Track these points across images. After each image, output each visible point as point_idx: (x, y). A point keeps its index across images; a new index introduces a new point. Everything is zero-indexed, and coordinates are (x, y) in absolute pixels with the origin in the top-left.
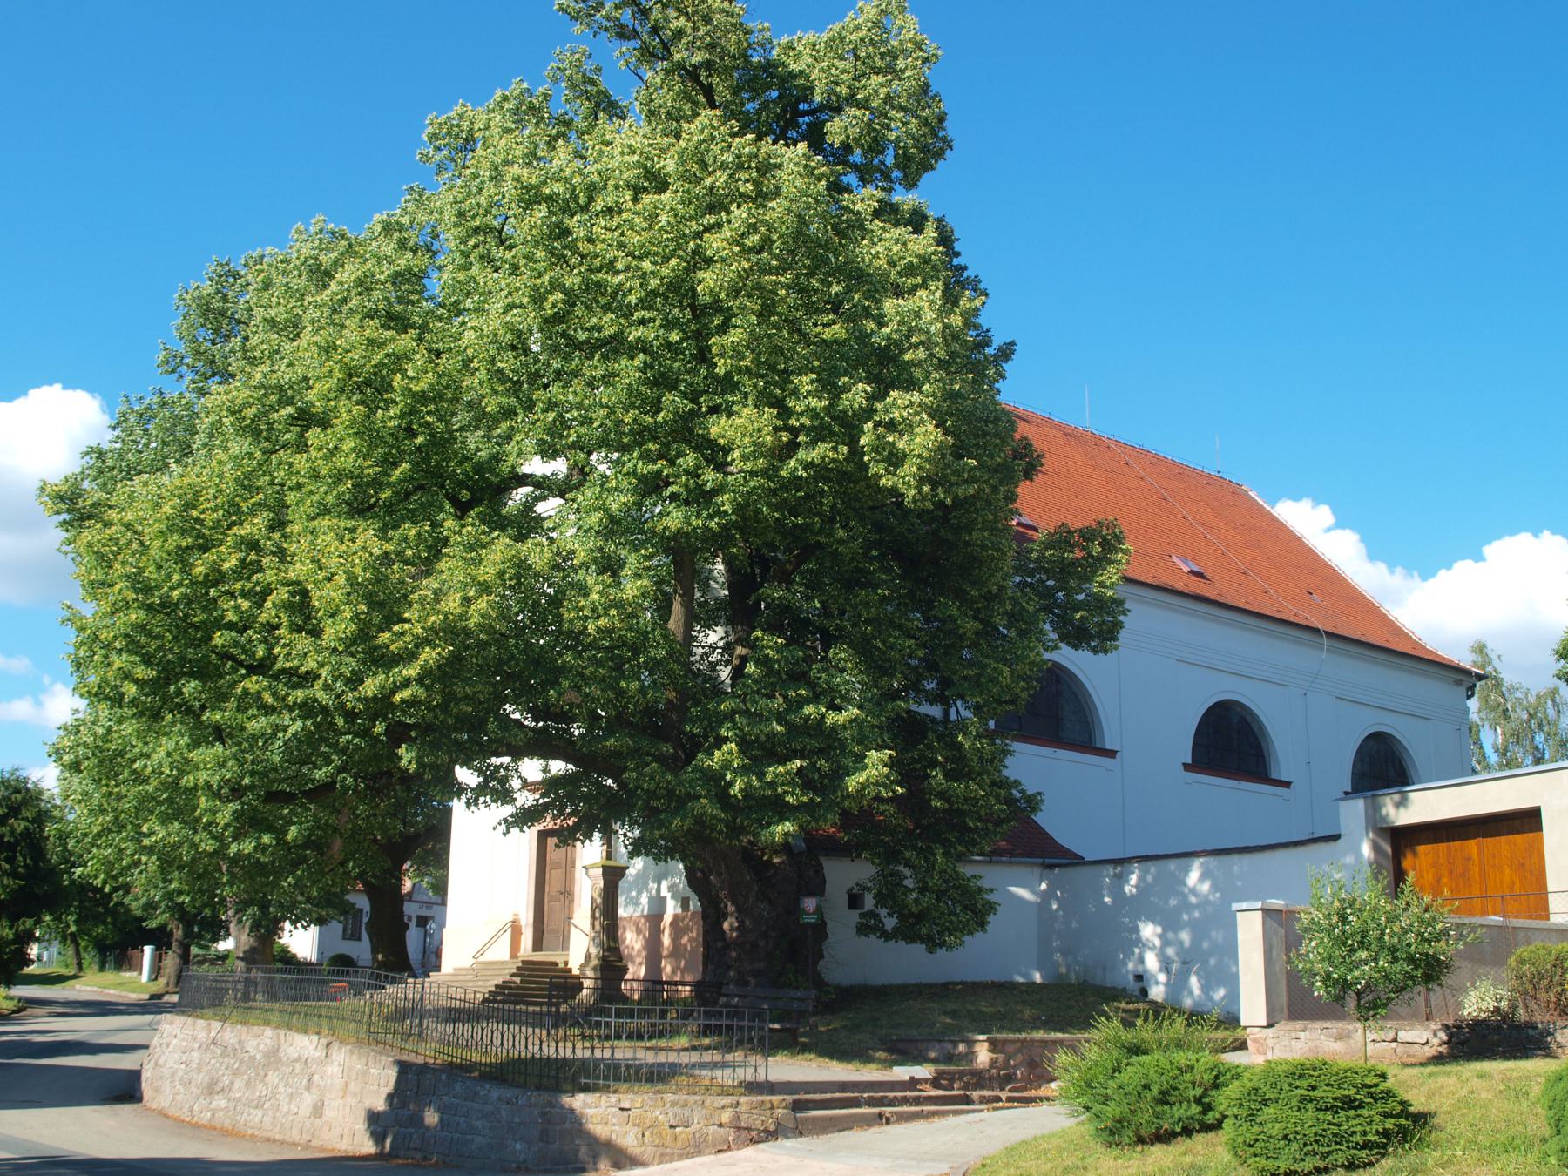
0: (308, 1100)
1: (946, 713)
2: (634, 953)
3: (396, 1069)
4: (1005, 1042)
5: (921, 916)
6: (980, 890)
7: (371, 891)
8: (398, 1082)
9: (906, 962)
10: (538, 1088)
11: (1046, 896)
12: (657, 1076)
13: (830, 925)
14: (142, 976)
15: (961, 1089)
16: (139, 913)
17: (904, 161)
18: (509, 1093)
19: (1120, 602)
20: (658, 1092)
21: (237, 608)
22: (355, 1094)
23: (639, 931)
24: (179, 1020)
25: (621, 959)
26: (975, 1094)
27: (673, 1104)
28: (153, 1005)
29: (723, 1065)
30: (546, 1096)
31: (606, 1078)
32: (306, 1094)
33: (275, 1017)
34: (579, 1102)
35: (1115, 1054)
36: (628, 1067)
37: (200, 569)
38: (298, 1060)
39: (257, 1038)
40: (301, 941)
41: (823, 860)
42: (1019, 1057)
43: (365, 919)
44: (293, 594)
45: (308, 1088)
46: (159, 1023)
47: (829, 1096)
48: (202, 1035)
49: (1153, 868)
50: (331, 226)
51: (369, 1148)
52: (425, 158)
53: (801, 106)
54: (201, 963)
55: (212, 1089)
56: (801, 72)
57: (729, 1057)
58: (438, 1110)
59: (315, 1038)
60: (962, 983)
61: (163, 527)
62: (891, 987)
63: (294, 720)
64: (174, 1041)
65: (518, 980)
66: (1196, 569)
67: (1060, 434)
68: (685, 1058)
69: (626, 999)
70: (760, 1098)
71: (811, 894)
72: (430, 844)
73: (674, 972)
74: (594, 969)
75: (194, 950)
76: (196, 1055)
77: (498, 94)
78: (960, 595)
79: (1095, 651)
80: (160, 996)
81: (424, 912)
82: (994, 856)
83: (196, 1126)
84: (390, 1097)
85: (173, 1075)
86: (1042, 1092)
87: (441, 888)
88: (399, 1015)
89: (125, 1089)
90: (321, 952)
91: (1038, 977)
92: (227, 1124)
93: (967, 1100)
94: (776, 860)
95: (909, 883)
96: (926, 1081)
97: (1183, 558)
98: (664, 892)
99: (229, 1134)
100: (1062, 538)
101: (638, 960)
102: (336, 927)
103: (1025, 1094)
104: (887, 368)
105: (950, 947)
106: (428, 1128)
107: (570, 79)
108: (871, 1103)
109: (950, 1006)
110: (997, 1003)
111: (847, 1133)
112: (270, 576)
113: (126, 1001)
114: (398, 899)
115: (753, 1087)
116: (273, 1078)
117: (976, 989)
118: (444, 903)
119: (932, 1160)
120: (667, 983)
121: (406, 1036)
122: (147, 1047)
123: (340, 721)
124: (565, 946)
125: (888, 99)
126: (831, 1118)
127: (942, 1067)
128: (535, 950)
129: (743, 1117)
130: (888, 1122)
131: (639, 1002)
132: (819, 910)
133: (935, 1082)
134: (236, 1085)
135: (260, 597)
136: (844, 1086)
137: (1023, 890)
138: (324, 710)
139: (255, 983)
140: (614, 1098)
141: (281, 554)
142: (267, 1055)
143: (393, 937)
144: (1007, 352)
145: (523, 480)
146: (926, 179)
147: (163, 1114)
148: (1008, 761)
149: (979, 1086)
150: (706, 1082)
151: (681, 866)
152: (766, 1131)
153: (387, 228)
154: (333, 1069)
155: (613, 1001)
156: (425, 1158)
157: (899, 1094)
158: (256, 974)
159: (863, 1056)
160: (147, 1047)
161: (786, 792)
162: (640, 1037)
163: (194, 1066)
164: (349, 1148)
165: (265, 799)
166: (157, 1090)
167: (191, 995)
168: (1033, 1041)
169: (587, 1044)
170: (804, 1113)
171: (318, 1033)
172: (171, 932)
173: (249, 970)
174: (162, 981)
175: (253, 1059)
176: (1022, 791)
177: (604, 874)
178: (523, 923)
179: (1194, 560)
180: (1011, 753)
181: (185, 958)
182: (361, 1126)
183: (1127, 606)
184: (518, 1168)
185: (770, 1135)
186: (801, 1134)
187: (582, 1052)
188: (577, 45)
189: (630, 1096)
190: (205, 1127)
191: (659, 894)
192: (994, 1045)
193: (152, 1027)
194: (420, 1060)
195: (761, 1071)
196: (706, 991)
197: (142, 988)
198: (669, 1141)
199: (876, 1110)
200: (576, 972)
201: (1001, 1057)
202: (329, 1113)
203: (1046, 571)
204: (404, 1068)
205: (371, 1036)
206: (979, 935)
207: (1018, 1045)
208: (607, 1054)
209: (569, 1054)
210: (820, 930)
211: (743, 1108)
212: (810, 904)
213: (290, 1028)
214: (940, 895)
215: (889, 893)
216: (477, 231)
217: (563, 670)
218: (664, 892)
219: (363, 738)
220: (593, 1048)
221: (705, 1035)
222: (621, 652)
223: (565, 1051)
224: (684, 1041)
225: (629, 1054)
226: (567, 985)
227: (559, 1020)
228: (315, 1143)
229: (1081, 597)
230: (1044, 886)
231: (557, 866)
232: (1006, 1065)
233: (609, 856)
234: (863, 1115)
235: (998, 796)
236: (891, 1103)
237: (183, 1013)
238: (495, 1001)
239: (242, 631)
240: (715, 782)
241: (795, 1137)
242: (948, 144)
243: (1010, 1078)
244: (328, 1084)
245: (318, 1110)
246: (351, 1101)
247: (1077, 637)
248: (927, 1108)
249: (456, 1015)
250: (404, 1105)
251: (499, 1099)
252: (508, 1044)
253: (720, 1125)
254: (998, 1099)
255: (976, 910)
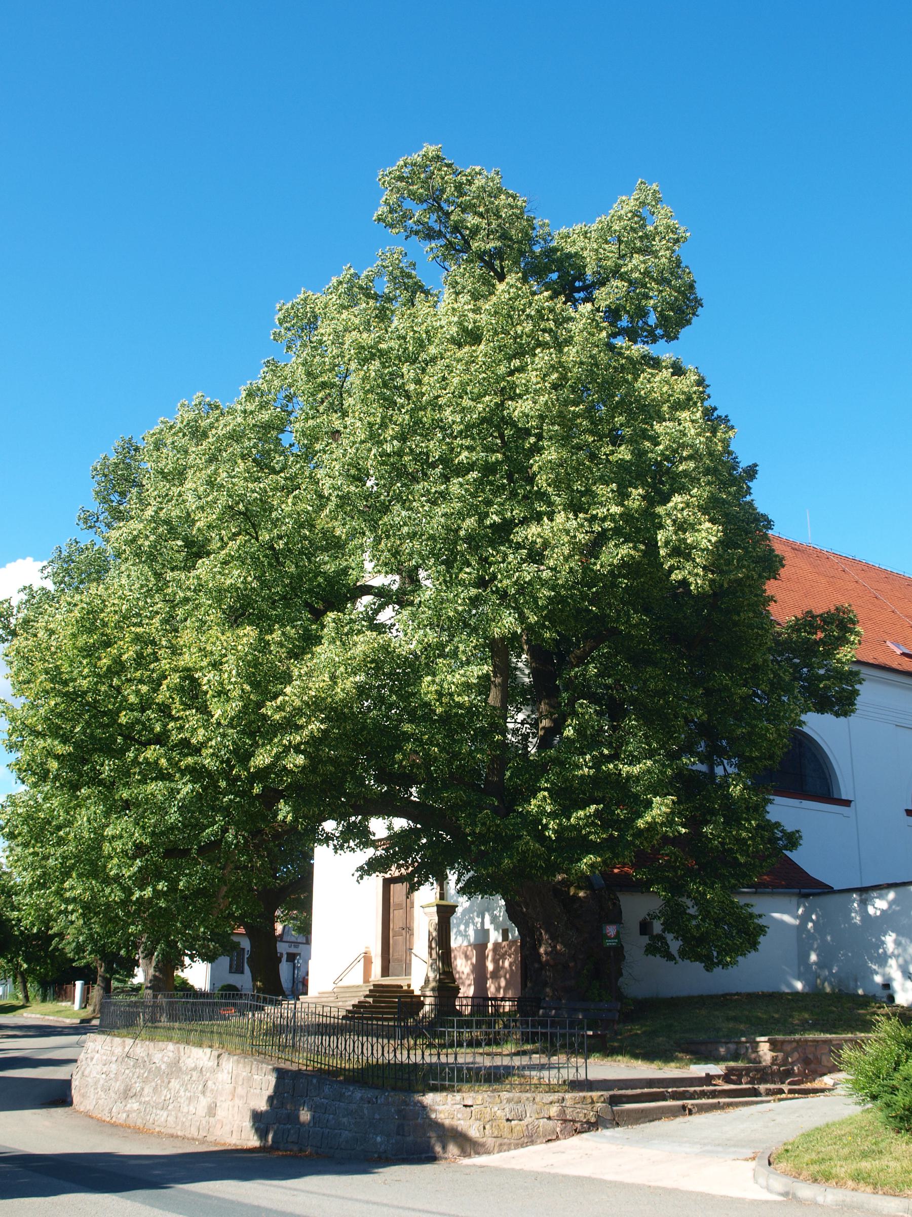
0: (204, 1102)
1: (712, 769)
2: (464, 977)
3: (275, 1075)
4: (783, 1042)
5: (702, 940)
6: (751, 916)
7: (252, 933)
8: (277, 1086)
9: (689, 978)
10: (394, 1089)
11: (805, 918)
12: (494, 1077)
13: (626, 948)
14: (72, 1008)
15: (750, 1084)
16: (71, 955)
17: (663, 319)
18: (370, 1094)
19: (857, 674)
20: (494, 1091)
21: (137, 692)
22: (241, 1097)
23: (467, 957)
24: (100, 1038)
25: (454, 981)
26: (762, 1087)
27: (509, 1101)
28: (82, 1028)
29: (549, 1067)
30: (402, 1096)
31: (451, 1079)
32: (201, 1097)
33: (176, 1034)
34: (429, 1099)
35: (895, 1048)
36: (469, 1069)
37: (105, 662)
38: (195, 1069)
39: (162, 1052)
40: (197, 974)
41: (618, 894)
42: (796, 1055)
43: (246, 956)
44: (183, 679)
45: (203, 1093)
46: (84, 1042)
47: (639, 1091)
48: (118, 1051)
49: (901, 889)
50: (208, 399)
51: (253, 1142)
52: (277, 336)
53: (577, 284)
54: (118, 994)
55: (127, 1094)
56: (576, 253)
57: (554, 1059)
58: (310, 1110)
59: (208, 1050)
60: (737, 994)
61: (75, 630)
62: (678, 998)
63: (185, 784)
64: (97, 1056)
65: (371, 1000)
66: (907, 651)
67: (789, 549)
68: (517, 1061)
69: (460, 1014)
70: (582, 1094)
71: (611, 922)
72: (297, 892)
73: (498, 989)
74: (433, 990)
75: (114, 984)
76: (114, 1067)
77: (334, 280)
78: (728, 668)
79: (837, 715)
80: (88, 1021)
81: (293, 950)
82: (759, 889)
83: (114, 1125)
84: (271, 1099)
85: (96, 1083)
86: (817, 1084)
87: (305, 929)
88: (277, 1030)
89: (58, 1096)
90: (213, 984)
91: (799, 986)
92: (139, 1123)
93: (756, 1093)
94: (581, 894)
95: (692, 911)
96: (719, 1077)
97: (897, 644)
98: (488, 925)
99: (139, 1131)
100: (809, 622)
101: (468, 982)
102: (224, 961)
103: (803, 1086)
104: (660, 480)
105: (726, 965)
106: (303, 1125)
107: (391, 273)
108: (675, 1096)
109: (732, 1013)
110: (771, 1010)
111: (656, 1123)
112: (165, 664)
113: (62, 1025)
114: (272, 939)
115: (576, 1085)
116: (175, 1084)
117: (753, 998)
118: (308, 942)
119: (734, 1146)
120: (492, 999)
121: (282, 1047)
122: (75, 1061)
123: (223, 784)
124: (408, 972)
125: (646, 273)
126: (643, 1111)
127: (732, 1064)
128: (382, 976)
129: (568, 1111)
130: (690, 1113)
131: (471, 1014)
132: (617, 936)
133: (727, 1078)
134: (146, 1091)
135: (156, 685)
136: (651, 1083)
137: (784, 915)
138: (210, 774)
139: (161, 1008)
140: (458, 1096)
141: (175, 651)
142: (169, 1065)
143: (269, 967)
144: (751, 473)
145: (367, 590)
146: (684, 332)
147: (88, 1116)
148: (769, 808)
149: (763, 1080)
150: (535, 1081)
151: (503, 902)
152: (588, 1122)
153: (250, 395)
154: (223, 1076)
155: (445, 1015)
156: (301, 1150)
157: (698, 1089)
158: (161, 999)
159: (666, 1057)
160: (75, 1061)
161: (590, 833)
162: (478, 1044)
163: (112, 1076)
164: (238, 1142)
165: (167, 852)
166: (83, 1096)
167: (113, 1019)
168: (806, 1041)
169: (434, 1051)
170: (619, 1107)
171: (211, 1047)
172: (96, 968)
173: (155, 997)
174: (90, 1009)
175: (159, 1068)
176: (783, 831)
177: (438, 912)
178: (373, 955)
179: (905, 645)
180: (770, 802)
181: (107, 989)
182: (247, 1124)
183: (862, 676)
184: (380, 1158)
185: (591, 1126)
186: (618, 1125)
187: (430, 1058)
188: (395, 248)
189: (472, 1094)
190: (121, 1125)
191: (482, 924)
192: (774, 1046)
193: (80, 1045)
194: (294, 1067)
195: (582, 1071)
196: (527, 1004)
197: (74, 1015)
198: (506, 1133)
199: (680, 1103)
200: (417, 992)
201: (780, 1055)
202: (221, 1113)
203: (793, 651)
204: (281, 1074)
205: (256, 1045)
206: (752, 955)
207: (794, 1044)
208: (451, 1060)
209: (419, 1060)
210: (618, 952)
211: (568, 1103)
212: (611, 930)
213: (188, 1043)
214: (717, 922)
215: (675, 918)
216: (324, 385)
217: (406, 737)
218: (488, 925)
219: (242, 797)
220: (439, 1055)
221: (527, 1042)
222: (452, 722)
223: (416, 1057)
224: (509, 1048)
225: (469, 1059)
226: (411, 1003)
227: (408, 1032)
228: (210, 1138)
229: (822, 672)
230: (800, 911)
231: (399, 906)
232: (785, 1062)
233: (442, 897)
234: (669, 1107)
235: (762, 837)
236: (692, 1096)
237: (103, 1032)
238: (353, 1018)
239: (143, 710)
240: (534, 824)
241: (613, 1127)
242: (699, 303)
243: (788, 1073)
244: (211, 1090)
245: (212, 1111)
246: (238, 1102)
247: (823, 705)
248: (723, 1100)
249: (324, 1029)
250: (282, 1104)
251: (361, 1098)
252: (367, 1052)
253: (549, 1118)
254: (781, 1091)
255: (749, 933)
